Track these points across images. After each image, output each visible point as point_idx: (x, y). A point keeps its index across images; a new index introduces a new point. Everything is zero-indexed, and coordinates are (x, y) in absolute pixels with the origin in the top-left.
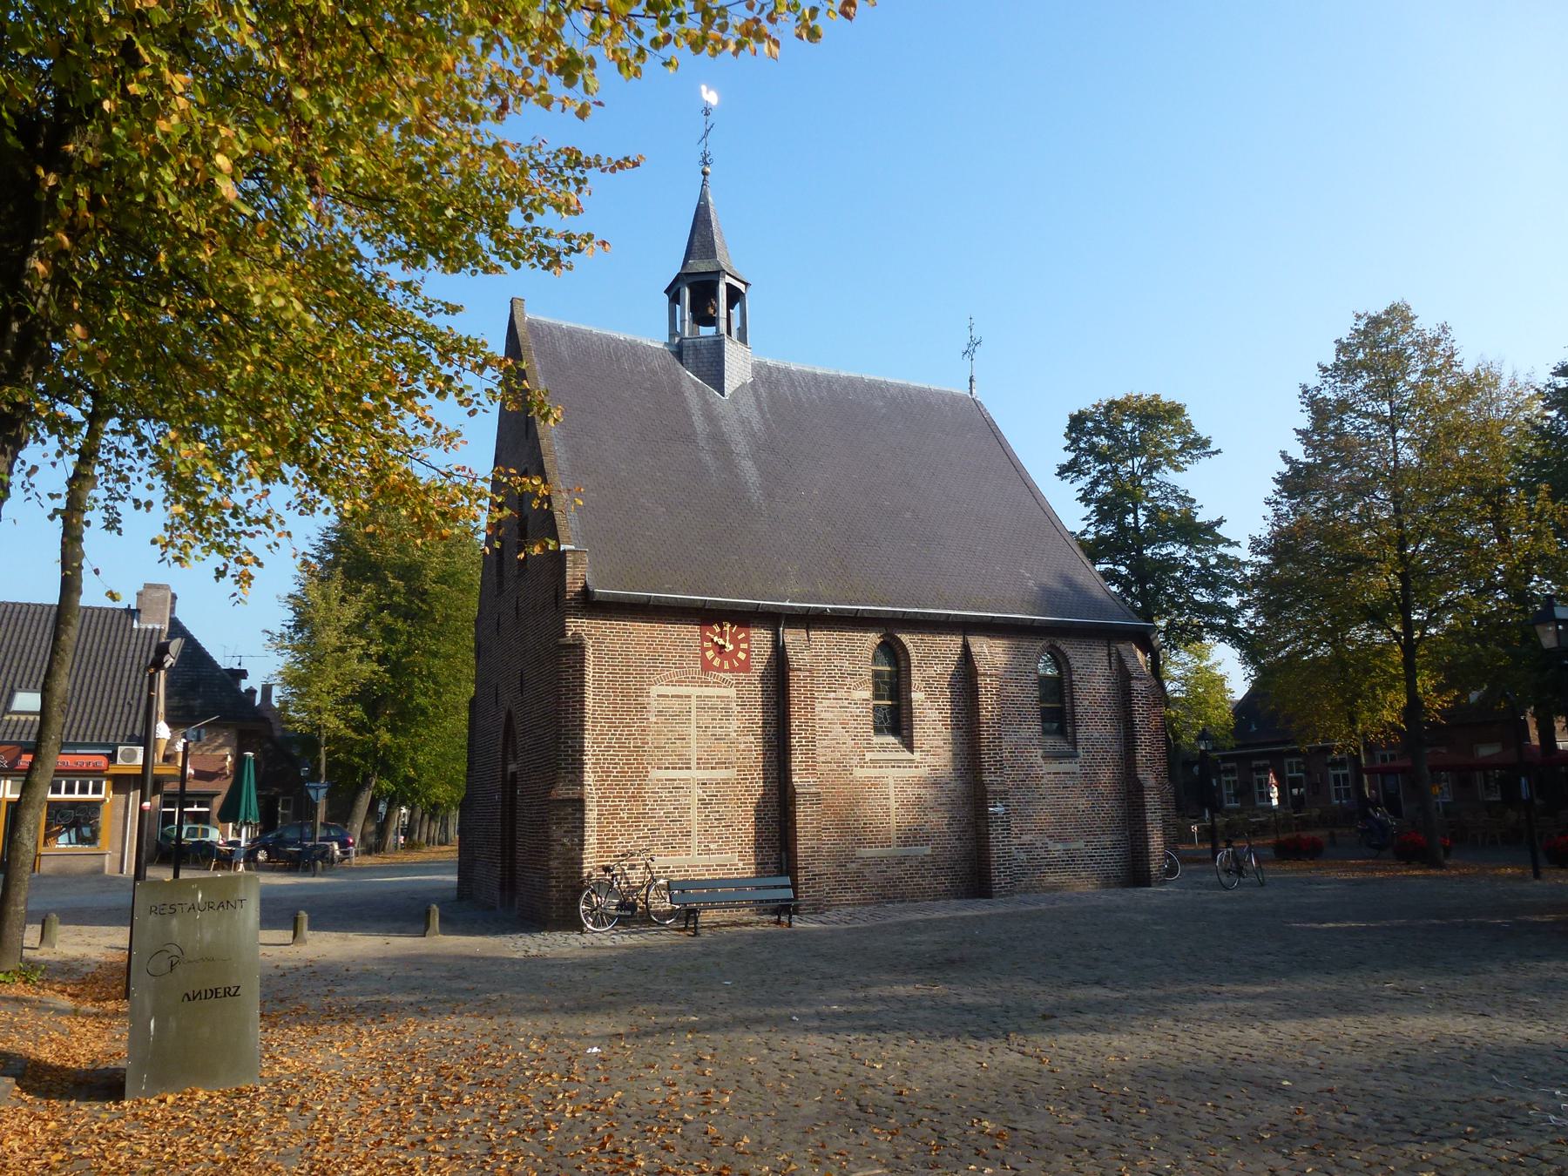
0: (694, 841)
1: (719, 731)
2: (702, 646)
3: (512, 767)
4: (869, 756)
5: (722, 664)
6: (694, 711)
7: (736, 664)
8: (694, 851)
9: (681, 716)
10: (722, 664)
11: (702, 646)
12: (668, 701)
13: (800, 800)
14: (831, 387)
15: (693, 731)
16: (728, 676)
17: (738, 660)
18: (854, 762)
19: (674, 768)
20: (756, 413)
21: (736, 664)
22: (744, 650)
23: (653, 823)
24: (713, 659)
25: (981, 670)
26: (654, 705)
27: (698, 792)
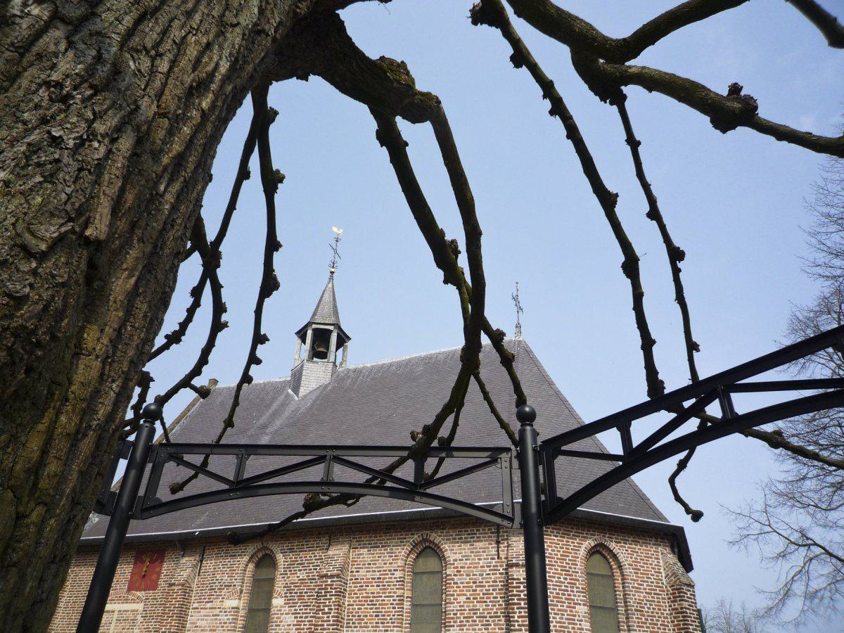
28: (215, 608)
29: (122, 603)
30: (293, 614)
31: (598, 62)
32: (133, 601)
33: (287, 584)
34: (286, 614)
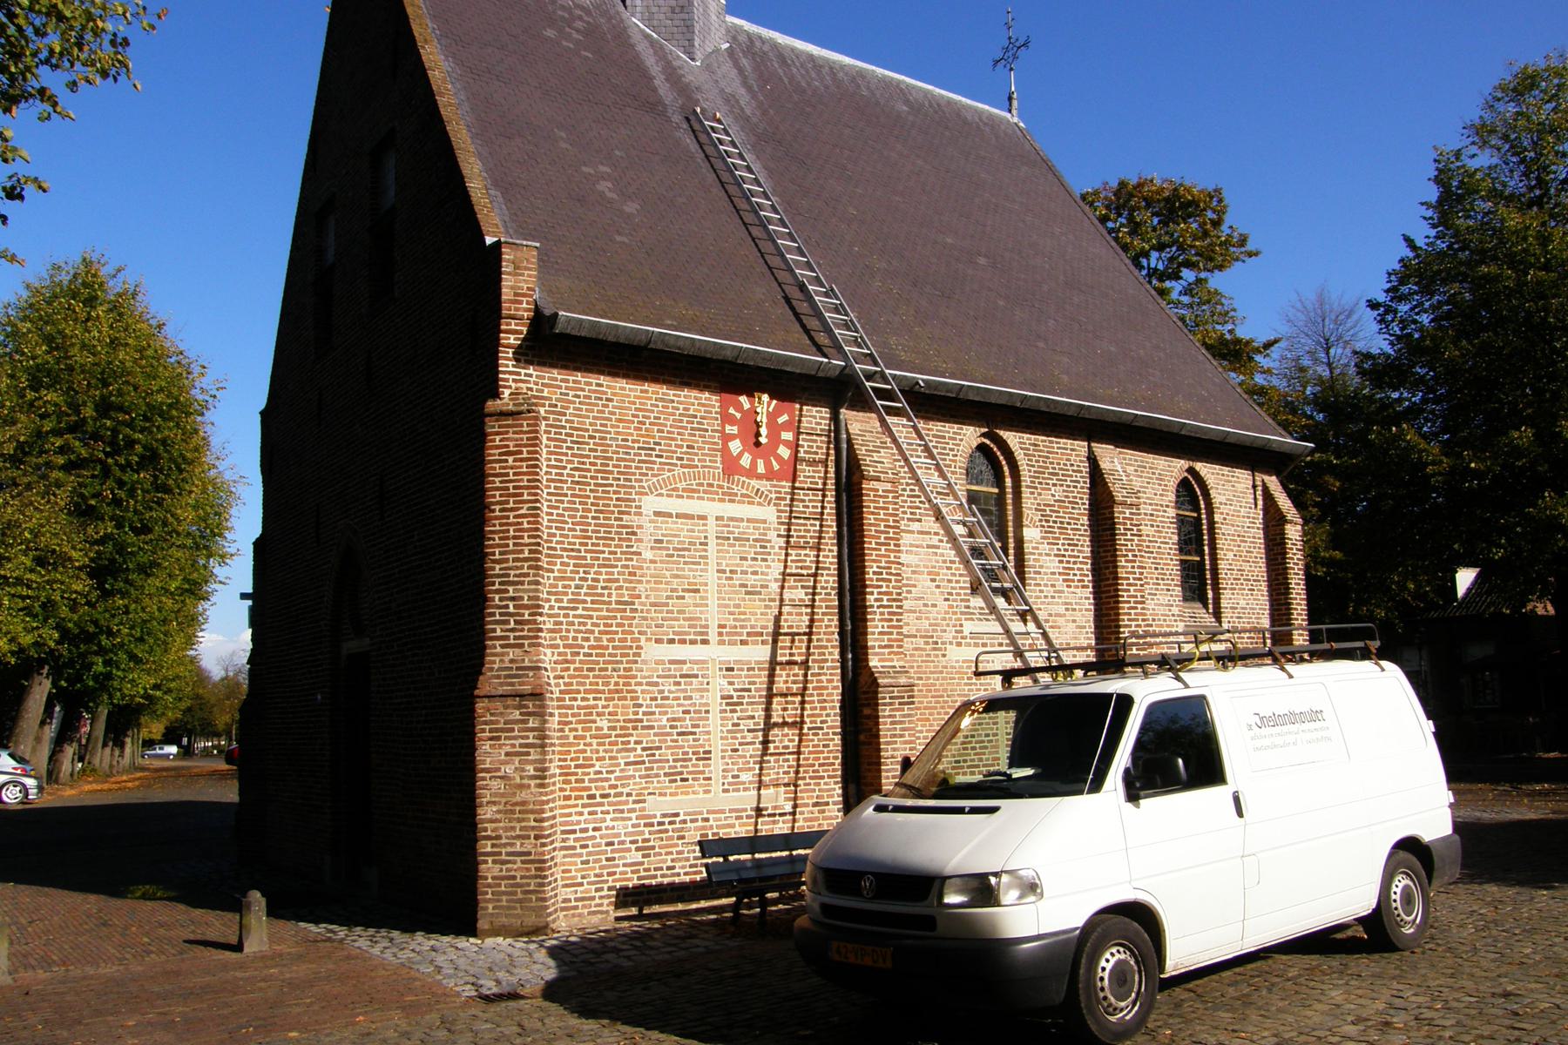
0: (716, 766)
1: (751, 580)
2: (723, 432)
3: (351, 646)
4: (968, 627)
5: (754, 464)
6: (712, 542)
7: (776, 466)
8: (716, 787)
9: (686, 552)
10: (754, 464)
11: (723, 432)
12: (671, 525)
13: (884, 697)
14: (834, 74)
15: (712, 577)
16: (764, 485)
17: (779, 459)
18: (949, 636)
19: (683, 642)
20: (743, 91)
21: (776, 466)
22: (786, 443)
23: (650, 738)
24: (740, 455)
25: (1119, 497)
26: (648, 529)
27: (719, 684)
28: (929, 533)
29: (721, 500)
30: (1056, 555)
31: (1325, 418)
32: (747, 499)
33: (1039, 504)
34: (1047, 555)
